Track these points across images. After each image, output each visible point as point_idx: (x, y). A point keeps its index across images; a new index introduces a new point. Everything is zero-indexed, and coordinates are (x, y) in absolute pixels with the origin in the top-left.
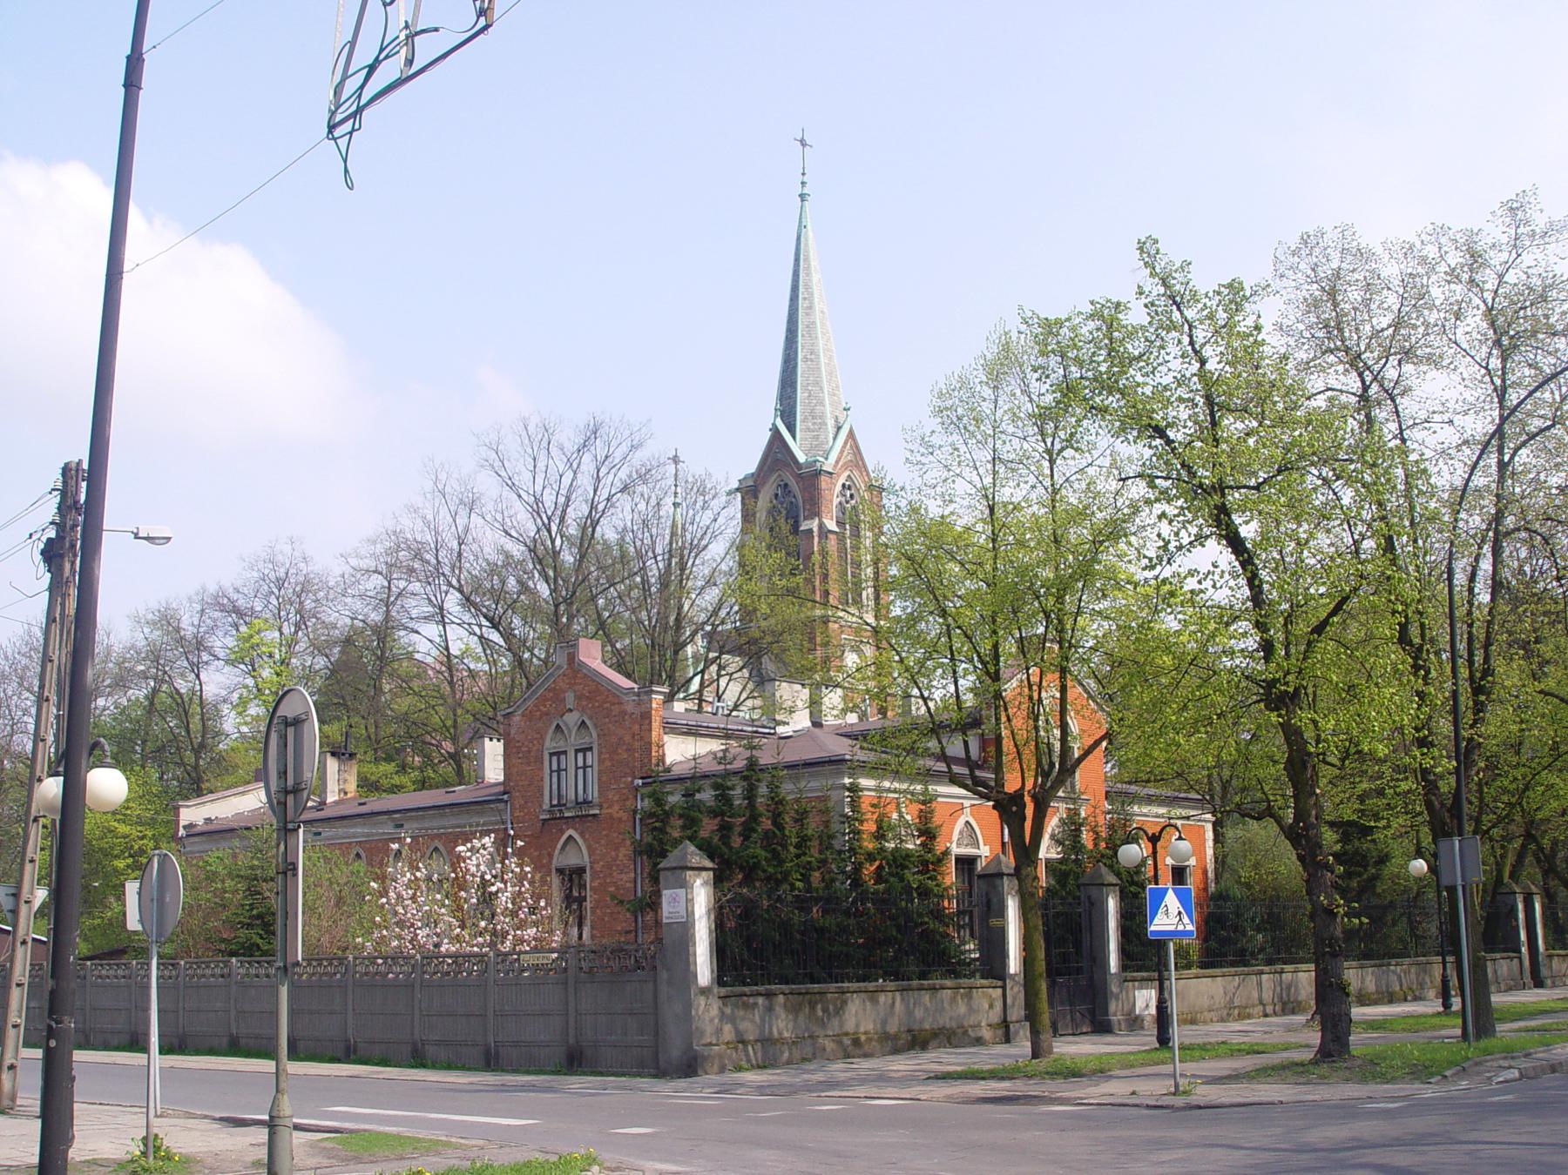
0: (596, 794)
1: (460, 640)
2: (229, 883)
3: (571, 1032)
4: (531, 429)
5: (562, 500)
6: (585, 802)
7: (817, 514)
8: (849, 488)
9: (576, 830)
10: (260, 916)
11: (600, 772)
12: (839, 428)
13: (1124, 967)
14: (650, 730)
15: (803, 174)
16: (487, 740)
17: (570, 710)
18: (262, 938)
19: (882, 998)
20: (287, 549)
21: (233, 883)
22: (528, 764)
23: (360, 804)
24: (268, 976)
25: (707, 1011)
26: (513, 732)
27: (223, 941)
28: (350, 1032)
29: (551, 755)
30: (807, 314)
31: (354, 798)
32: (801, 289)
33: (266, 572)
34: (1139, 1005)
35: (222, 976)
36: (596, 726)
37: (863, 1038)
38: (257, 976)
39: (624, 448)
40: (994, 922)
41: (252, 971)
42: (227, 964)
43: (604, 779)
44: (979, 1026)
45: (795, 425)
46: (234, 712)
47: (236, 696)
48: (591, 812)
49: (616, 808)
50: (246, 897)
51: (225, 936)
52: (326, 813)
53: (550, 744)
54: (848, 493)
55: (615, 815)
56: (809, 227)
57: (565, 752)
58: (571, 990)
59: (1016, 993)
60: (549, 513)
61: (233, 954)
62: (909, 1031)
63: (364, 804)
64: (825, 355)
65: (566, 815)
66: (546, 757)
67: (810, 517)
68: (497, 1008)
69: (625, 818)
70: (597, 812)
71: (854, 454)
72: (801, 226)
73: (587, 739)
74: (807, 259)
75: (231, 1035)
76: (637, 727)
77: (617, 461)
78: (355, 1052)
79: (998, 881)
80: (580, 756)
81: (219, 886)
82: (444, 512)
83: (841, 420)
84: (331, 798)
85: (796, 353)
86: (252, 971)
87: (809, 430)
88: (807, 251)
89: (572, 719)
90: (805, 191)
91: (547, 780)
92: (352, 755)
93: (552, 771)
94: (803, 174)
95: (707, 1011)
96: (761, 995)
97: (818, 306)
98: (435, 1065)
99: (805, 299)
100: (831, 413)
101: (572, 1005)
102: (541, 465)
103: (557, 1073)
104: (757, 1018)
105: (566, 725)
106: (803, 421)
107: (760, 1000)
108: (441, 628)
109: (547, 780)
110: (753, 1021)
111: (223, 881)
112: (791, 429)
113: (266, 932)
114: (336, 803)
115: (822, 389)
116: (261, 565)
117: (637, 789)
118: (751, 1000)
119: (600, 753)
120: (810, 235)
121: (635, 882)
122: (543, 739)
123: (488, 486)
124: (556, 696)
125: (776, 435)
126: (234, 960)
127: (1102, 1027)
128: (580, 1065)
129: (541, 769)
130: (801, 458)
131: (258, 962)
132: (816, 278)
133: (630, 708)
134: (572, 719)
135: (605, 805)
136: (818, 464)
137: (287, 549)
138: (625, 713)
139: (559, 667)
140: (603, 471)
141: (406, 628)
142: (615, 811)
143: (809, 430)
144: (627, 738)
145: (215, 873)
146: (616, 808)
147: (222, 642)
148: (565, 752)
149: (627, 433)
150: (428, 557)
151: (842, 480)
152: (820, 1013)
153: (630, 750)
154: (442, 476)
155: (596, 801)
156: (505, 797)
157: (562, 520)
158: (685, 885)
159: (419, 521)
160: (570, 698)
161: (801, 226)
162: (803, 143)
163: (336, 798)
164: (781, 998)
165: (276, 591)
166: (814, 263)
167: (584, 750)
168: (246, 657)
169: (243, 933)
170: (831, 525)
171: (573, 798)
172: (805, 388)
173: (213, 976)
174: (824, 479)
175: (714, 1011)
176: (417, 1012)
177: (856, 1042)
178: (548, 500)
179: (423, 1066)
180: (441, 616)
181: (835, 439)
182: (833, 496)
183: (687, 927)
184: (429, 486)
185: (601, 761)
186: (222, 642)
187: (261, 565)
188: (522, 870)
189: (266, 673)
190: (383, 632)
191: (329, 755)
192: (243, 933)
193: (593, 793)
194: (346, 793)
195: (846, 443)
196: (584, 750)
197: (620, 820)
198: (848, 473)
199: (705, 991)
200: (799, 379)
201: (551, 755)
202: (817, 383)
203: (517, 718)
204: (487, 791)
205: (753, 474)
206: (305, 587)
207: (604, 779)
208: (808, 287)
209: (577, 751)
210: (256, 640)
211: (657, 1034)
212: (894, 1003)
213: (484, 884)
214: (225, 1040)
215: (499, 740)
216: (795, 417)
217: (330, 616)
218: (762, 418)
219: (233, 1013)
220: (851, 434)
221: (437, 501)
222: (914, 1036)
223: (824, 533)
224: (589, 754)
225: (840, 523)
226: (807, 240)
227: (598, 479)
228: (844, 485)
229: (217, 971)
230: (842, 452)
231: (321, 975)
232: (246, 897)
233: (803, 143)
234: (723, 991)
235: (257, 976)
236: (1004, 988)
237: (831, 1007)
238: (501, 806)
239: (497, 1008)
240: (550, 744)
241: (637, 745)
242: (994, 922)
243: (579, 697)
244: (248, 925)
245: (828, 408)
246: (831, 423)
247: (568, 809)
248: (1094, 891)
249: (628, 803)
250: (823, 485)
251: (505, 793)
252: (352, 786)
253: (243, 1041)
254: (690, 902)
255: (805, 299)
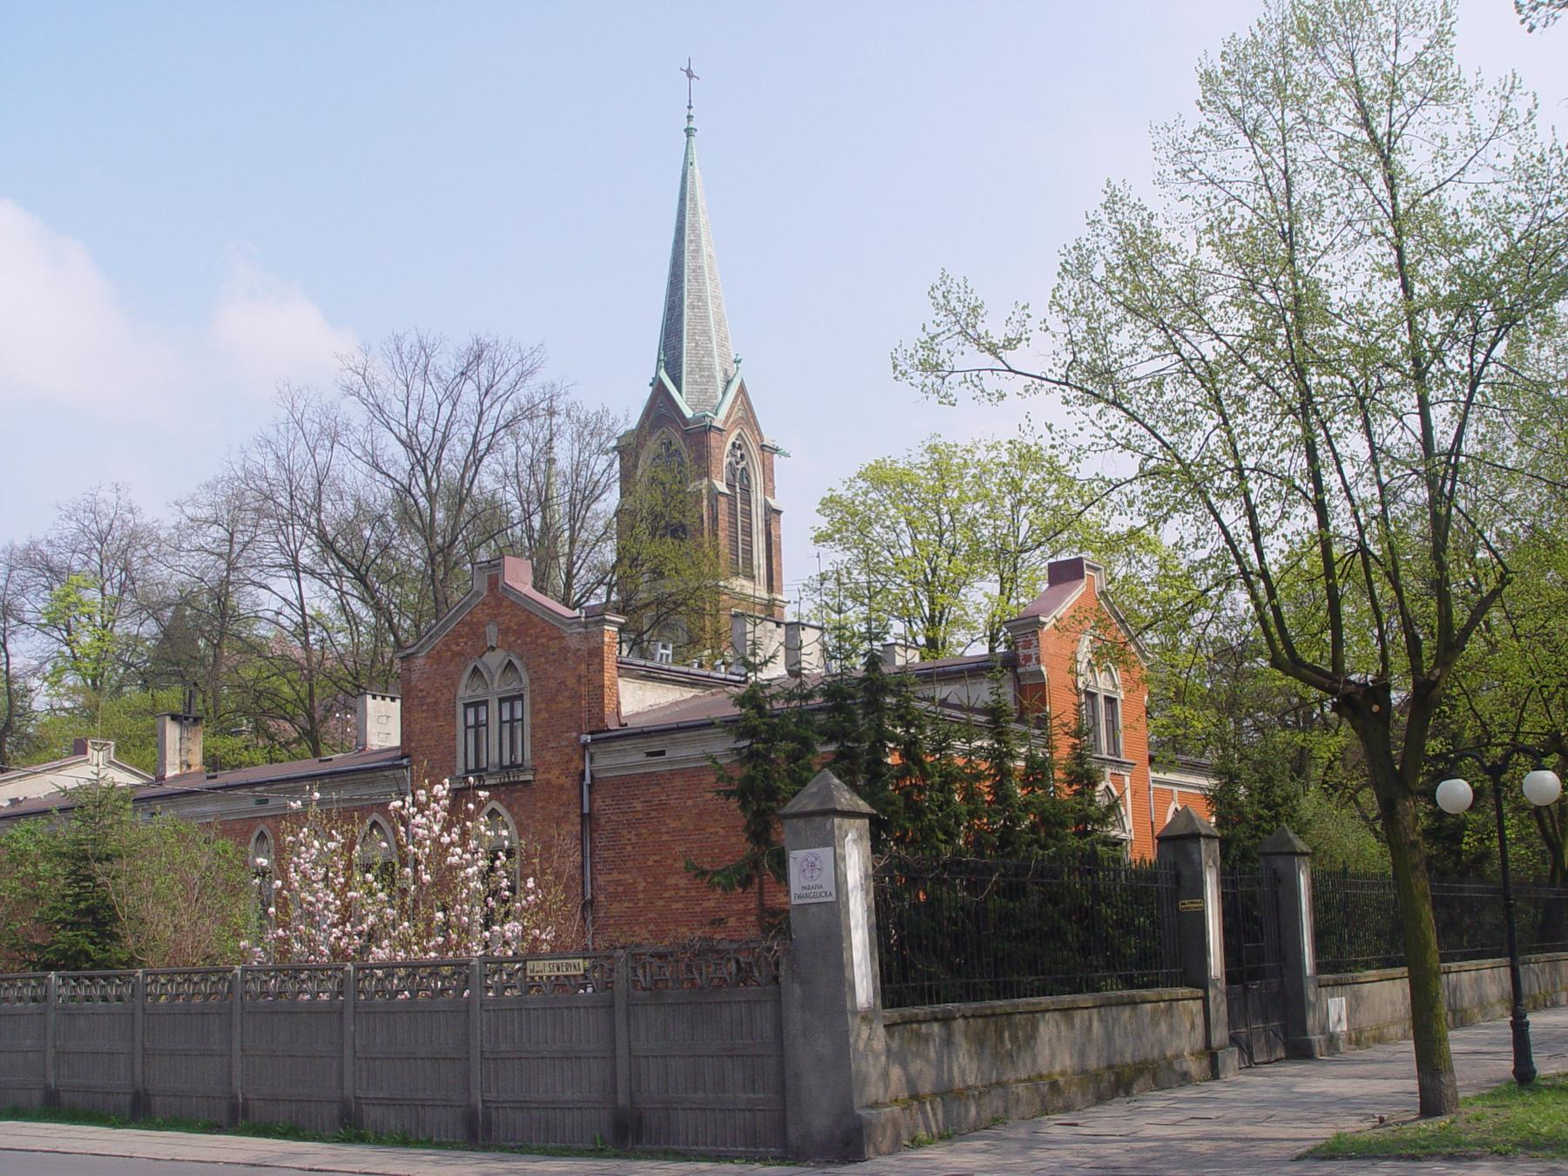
0: (528, 755)
1: (319, 599)
2: (42, 866)
3: (622, 1087)
4: (405, 349)
5: (439, 435)
6: (513, 765)
7: (707, 474)
8: (740, 447)
9: (501, 802)
10: (90, 911)
11: (533, 727)
12: (728, 382)
13: (1320, 968)
14: (602, 670)
15: (690, 107)
16: (369, 698)
17: (493, 649)
18: (93, 943)
19: (1079, 1017)
20: (112, 498)
21: (49, 866)
22: (436, 718)
23: (209, 778)
24: (105, 999)
25: (869, 1040)
26: (414, 677)
27: (35, 948)
28: (237, 1084)
29: (467, 706)
30: (694, 258)
31: (200, 772)
32: (687, 231)
33: (86, 523)
34: (1333, 1017)
35: (34, 999)
36: (527, 666)
37: (1061, 1081)
38: (88, 998)
39: (512, 375)
40: (1186, 904)
41: (82, 992)
42: (41, 982)
43: (539, 735)
44: (1179, 1056)
45: (680, 378)
46: (46, 684)
47: (48, 667)
48: (522, 778)
49: (556, 771)
50: (69, 885)
51: (38, 941)
52: (169, 788)
53: (464, 692)
54: (739, 453)
55: (554, 781)
56: (696, 164)
57: (485, 703)
58: (620, 1017)
59: (1218, 996)
60: (424, 450)
61: (48, 967)
62: (1110, 1067)
63: (215, 777)
64: (713, 303)
65: (487, 783)
66: (460, 710)
67: (700, 477)
68: (487, 1047)
69: (568, 785)
70: (531, 778)
71: (745, 410)
72: (687, 163)
73: (515, 685)
74: (693, 198)
75: (47, 1088)
76: (583, 666)
77: (500, 393)
78: (246, 1115)
79: (1191, 846)
80: (506, 707)
81: (30, 870)
82: (301, 448)
83: (731, 373)
84: (171, 772)
85: (682, 300)
86: (82, 992)
87: (696, 383)
88: (694, 190)
89: (495, 660)
90: (692, 125)
91: (461, 738)
92: (197, 720)
93: (467, 727)
94: (690, 107)
95: (869, 1040)
96: (936, 1020)
97: (705, 250)
98: (379, 1139)
99: (691, 241)
100: (720, 365)
101: (622, 1043)
102: (415, 395)
103: (598, 1153)
104: (932, 1055)
105: (487, 667)
106: (690, 373)
107: (936, 1027)
108: (295, 583)
109: (461, 738)
110: (927, 1060)
111: (35, 865)
112: (677, 382)
113: (102, 934)
114: (176, 777)
115: (710, 339)
116: (81, 514)
117: (585, 746)
118: (924, 1028)
119: (533, 704)
120: (697, 172)
121: (583, 866)
122: (455, 685)
123: (355, 413)
124: (474, 631)
125: (659, 388)
126: (52, 975)
127: (1300, 1051)
128: (638, 1140)
129: (453, 725)
130: (688, 413)
131: (91, 979)
132: (704, 219)
133: (573, 643)
134: (495, 660)
135: (541, 769)
136: (708, 420)
137: (112, 498)
138: (566, 649)
139: (478, 594)
140: (487, 403)
141: (253, 583)
142: (555, 776)
143: (696, 383)
144: (571, 682)
145: (24, 854)
146: (556, 771)
147: (33, 605)
148: (485, 703)
149: (517, 357)
150: (281, 500)
151: (732, 439)
152: (1008, 1045)
153: (576, 696)
154: (300, 404)
155: (528, 763)
156: (405, 761)
157: (438, 459)
158: (829, 840)
159: (271, 456)
160: (492, 633)
161: (687, 163)
162: (690, 74)
163: (177, 772)
164: (959, 1024)
165: (98, 546)
166: (701, 203)
167: (512, 699)
168: (59, 620)
169: (64, 936)
170: (722, 487)
171: (497, 760)
172: (692, 338)
173: (20, 999)
174: (713, 435)
175: (879, 1044)
176: (348, 1052)
177: (1054, 1085)
178: (425, 430)
179: (359, 1138)
180: (296, 568)
181: (724, 393)
182: (722, 455)
183: (836, 911)
184: (283, 414)
185: (535, 713)
186: (33, 605)
187: (81, 514)
188: (496, 833)
189: (86, 639)
190: (221, 595)
191: (168, 718)
192: (64, 936)
193: (525, 753)
194: (189, 766)
195: (736, 398)
196: (512, 699)
197: (562, 788)
198: (738, 431)
199: (867, 1017)
200: (685, 328)
201: (467, 706)
202: (705, 332)
203: (420, 661)
204: (374, 758)
205: (633, 431)
206: (134, 536)
207: (539, 735)
208: (694, 229)
209: (501, 701)
210: (73, 599)
211: (782, 1084)
212: (1091, 1025)
213: (442, 851)
214: (37, 1097)
215: (393, 699)
216: (681, 369)
217: (160, 571)
218: (644, 366)
219: (51, 1053)
220: (742, 389)
221: (292, 433)
222: (1118, 1075)
223: (715, 495)
224: (518, 704)
225: (730, 486)
226: (693, 178)
227: (481, 414)
228: (734, 444)
229: (27, 992)
230: (732, 408)
231: (207, 997)
232: (69, 885)
233: (690, 74)
234: (894, 1014)
235: (88, 998)
236: (1205, 1000)
237: (1020, 1034)
238: (398, 773)
239: (487, 1047)
240: (464, 692)
241: (584, 690)
242: (1186, 904)
243: (504, 632)
244: (73, 923)
245: (717, 361)
246: (720, 376)
247: (492, 774)
248: (1280, 863)
249: (574, 765)
250: (713, 443)
251: (402, 758)
252: (197, 759)
253: (65, 1097)
254: (838, 861)
255: (691, 241)
